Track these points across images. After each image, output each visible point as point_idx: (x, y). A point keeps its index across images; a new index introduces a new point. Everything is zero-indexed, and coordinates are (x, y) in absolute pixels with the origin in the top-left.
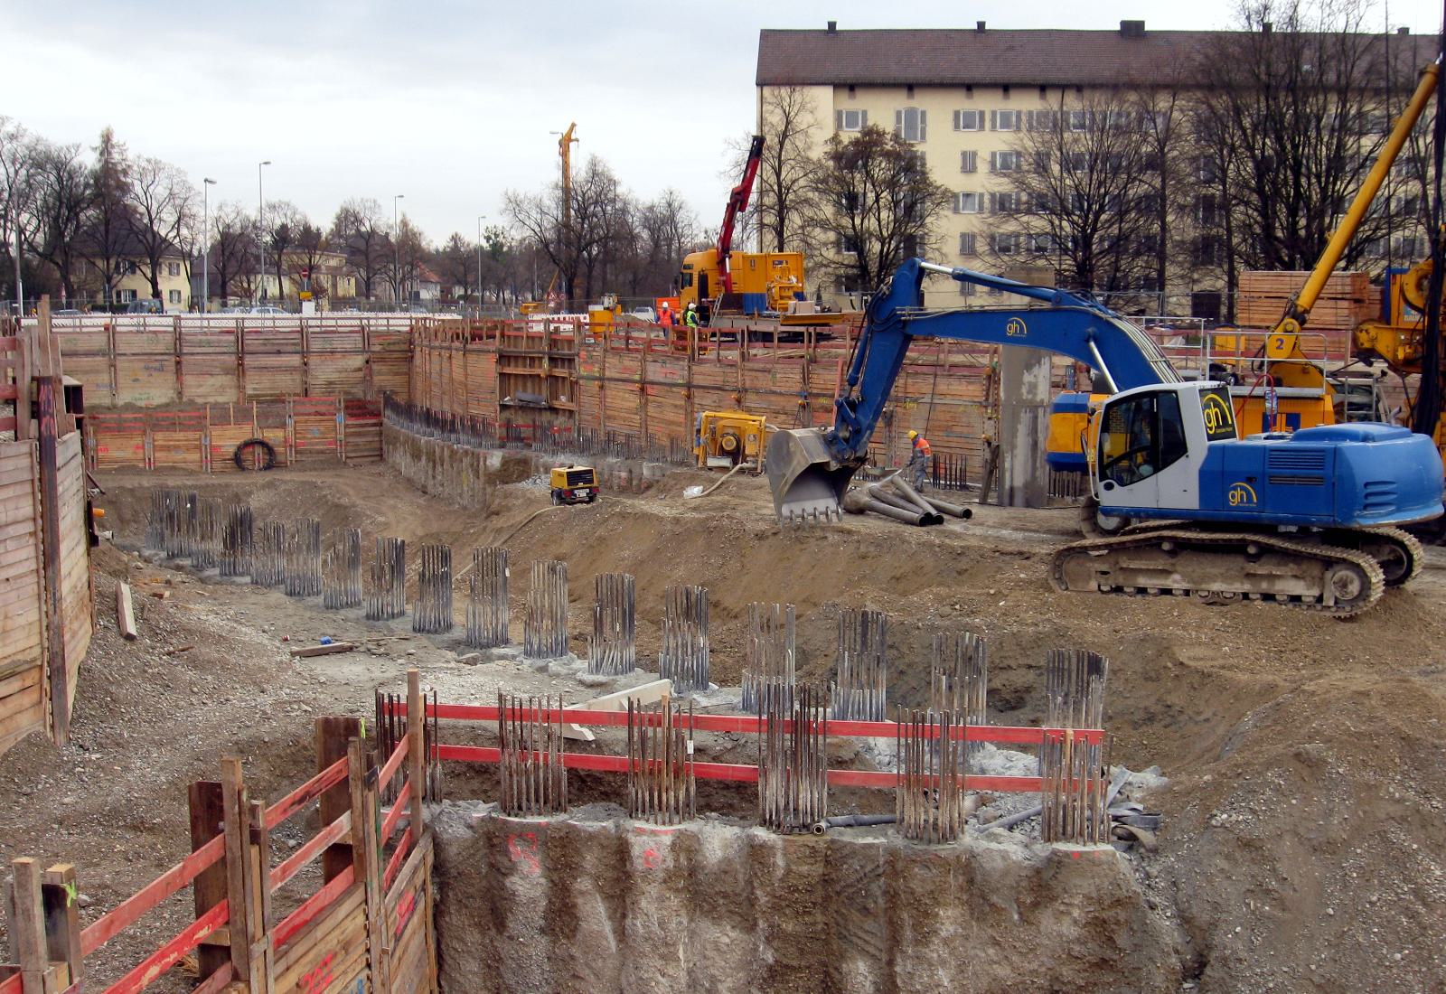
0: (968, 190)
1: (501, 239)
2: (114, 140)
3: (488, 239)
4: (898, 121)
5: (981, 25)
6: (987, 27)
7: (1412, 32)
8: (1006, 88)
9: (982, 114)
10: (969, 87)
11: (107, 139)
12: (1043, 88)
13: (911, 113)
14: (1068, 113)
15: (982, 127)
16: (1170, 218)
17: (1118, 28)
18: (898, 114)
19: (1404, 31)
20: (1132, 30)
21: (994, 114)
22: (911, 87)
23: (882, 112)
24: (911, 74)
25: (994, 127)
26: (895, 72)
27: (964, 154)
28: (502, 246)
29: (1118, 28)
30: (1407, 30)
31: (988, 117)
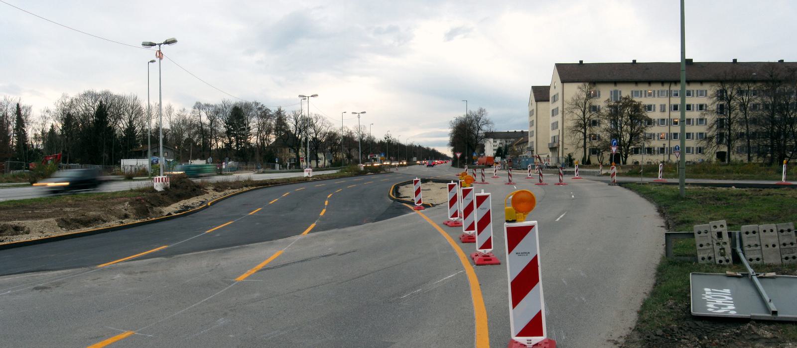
0: (663, 118)
1: (390, 139)
2: (21, 107)
3: (386, 138)
4: (611, 94)
5: (581, 62)
6: (738, 61)
7: (784, 61)
8: (650, 82)
9: (641, 91)
10: (637, 82)
11: (18, 105)
12: (663, 82)
13: (616, 92)
14: (672, 91)
15: (693, 96)
16: (210, 128)
17: (632, 62)
18: (611, 92)
19: (634, 61)
20: (782, 61)
21: (658, 91)
22: (615, 83)
23: (626, 91)
24: (650, 78)
25: (697, 96)
26: (609, 77)
27: (661, 105)
28: (390, 141)
29: (632, 62)
30: (636, 60)
31: (643, 93)
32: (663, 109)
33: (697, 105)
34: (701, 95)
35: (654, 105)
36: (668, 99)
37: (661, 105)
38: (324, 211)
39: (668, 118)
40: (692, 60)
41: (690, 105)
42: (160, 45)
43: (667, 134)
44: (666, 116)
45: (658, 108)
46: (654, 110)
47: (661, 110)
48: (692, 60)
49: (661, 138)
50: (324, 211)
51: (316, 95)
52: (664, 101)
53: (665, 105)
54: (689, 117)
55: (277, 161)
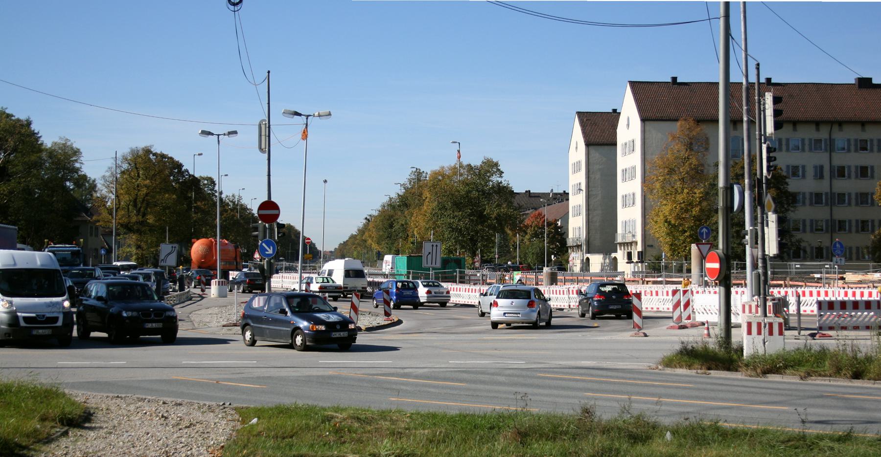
27: (815, 167)
32: (819, 173)
33: (856, 167)
34: (864, 149)
35: (804, 167)
36: (827, 154)
37: (815, 167)
38: (75, 327)
39: (829, 191)
40: (871, 79)
41: (843, 168)
42: (308, 116)
43: (827, 221)
44: (823, 186)
45: (810, 172)
46: (804, 176)
47: (815, 176)
48: (871, 79)
49: (817, 230)
50: (75, 327)
51: (235, 132)
52: (821, 158)
53: (822, 167)
54: (841, 191)
55: (75, 316)
